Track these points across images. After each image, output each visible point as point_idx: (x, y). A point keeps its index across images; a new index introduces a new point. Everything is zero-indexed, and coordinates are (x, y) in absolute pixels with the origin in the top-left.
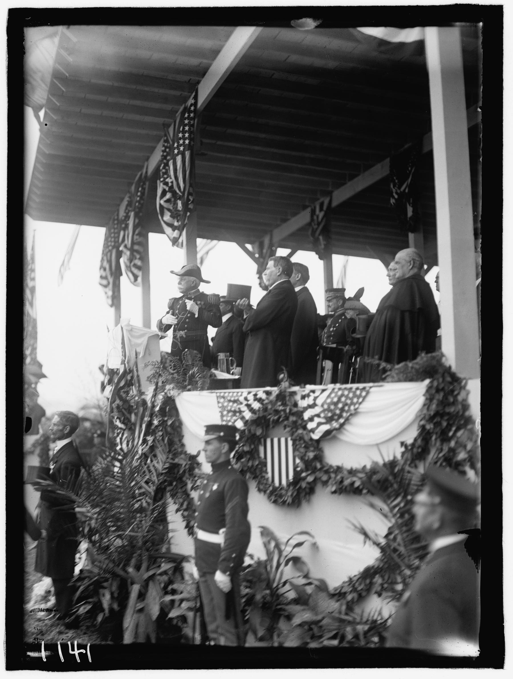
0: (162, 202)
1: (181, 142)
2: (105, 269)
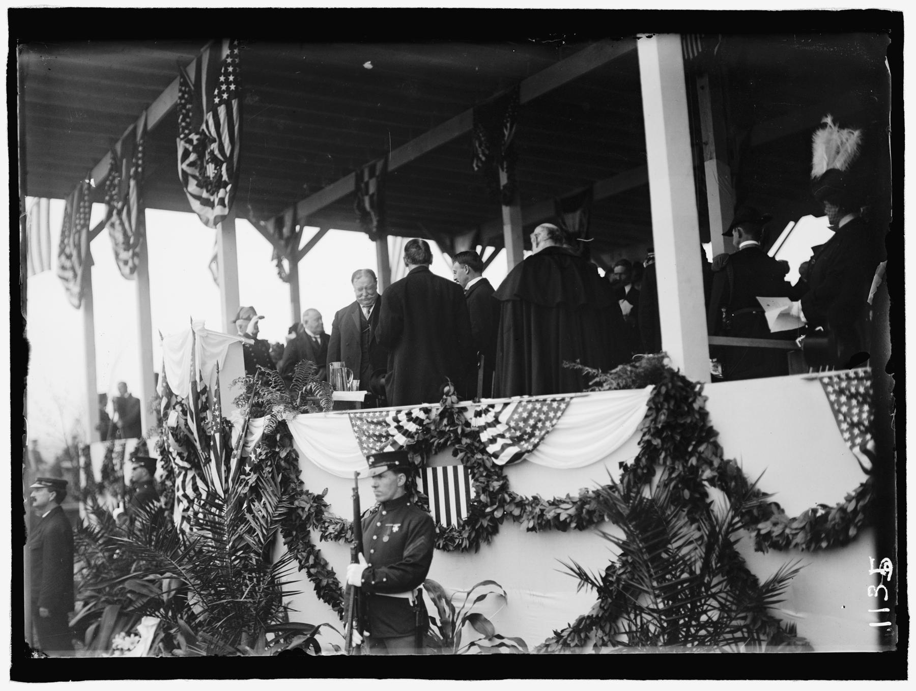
0: (184, 166)
1: (224, 87)
2: (69, 257)
